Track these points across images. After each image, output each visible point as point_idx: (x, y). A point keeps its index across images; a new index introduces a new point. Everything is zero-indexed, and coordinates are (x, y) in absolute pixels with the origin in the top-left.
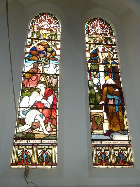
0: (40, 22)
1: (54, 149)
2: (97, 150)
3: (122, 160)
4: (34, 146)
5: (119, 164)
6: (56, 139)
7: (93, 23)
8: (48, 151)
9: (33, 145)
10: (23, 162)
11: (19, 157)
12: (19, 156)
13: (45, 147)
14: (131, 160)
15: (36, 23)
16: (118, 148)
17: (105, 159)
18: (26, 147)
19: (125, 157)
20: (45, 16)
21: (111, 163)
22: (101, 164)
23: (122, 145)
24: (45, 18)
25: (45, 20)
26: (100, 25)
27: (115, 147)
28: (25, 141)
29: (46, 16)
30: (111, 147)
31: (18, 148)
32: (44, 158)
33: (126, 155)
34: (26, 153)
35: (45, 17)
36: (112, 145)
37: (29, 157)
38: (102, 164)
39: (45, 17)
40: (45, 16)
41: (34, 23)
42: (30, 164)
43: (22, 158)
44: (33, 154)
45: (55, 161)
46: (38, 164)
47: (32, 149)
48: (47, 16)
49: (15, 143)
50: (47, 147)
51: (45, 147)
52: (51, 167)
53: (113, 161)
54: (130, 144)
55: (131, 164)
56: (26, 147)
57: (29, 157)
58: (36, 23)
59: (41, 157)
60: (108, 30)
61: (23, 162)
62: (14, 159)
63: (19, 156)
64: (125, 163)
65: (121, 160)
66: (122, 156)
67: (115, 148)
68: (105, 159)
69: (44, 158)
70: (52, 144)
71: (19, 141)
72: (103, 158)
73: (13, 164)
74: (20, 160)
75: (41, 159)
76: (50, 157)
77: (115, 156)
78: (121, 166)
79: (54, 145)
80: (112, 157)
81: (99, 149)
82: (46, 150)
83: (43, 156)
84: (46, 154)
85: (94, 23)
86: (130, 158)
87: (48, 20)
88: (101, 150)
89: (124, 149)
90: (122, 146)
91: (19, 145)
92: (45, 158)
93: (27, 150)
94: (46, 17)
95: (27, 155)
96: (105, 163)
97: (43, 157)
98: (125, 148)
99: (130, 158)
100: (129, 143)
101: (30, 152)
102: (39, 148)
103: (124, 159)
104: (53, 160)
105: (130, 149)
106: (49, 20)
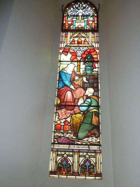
0: (73, 10)
1: (98, 156)
2: (80, 156)
3: (87, 169)
4: (74, 152)
5: (83, 174)
6: (100, 145)
7: (87, 6)
8: (91, 158)
9: (73, 151)
10: (63, 171)
11: (58, 164)
12: (58, 163)
13: (87, 154)
14: (100, 170)
15: (70, 12)
16: (63, 153)
17: (67, 167)
18: (65, 153)
19: (92, 166)
20: (79, 3)
21: (74, 172)
22: (61, 172)
23: (63, 150)
24: (79, 6)
25: (79, 8)
26: (82, 8)
27: (59, 151)
28: (66, 147)
29: (80, 4)
30: (54, 151)
31: (79, 155)
32: (87, 167)
33: (93, 163)
34: (65, 160)
35: (79, 5)
36: (77, 151)
37: (69, 165)
38: (62, 173)
39: (79, 5)
40: (79, 3)
41: (68, 13)
42: (71, 174)
43: (62, 166)
44: (74, 162)
45: (55, 169)
46: (80, 174)
47: (80, 156)
48: (82, 4)
49: (53, 148)
50: (67, 153)
51: (87, 154)
52: (86, 178)
53: (76, 170)
54: (100, 150)
55: (100, 175)
56: (65, 153)
57: (69, 165)
58: (70, 12)
59: (83, 166)
60: (90, 13)
61: (93, 171)
62: (52, 166)
63: (58, 163)
64: (90, 174)
65: (86, 170)
66: (89, 164)
67: (59, 153)
68: (67, 167)
69: (87, 167)
70: (95, 150)
71: (56, 147)
72: (63, 166)
73: (52, 173)
74: (83, 169)
75: (84, 168)
76: (94, 166)
77: (57, 162)
78: (66, 176)
79: (98, 151)
80: (76, 165)
81: (61, 154)
82: (89, 158)
83: (86, 164)
84: (89, 162)
85: (75, 6)
86: (99, 166)
87: (82, 8)
88: (63, 156)
89: (70, 155)
90: (68, 152)
91: (58, 150)
92: (88, 167)
93: (67, 157)
94: (81, 5)
95: (90, 162)
96: (65, 171)
97: (86, 166)
98: (71, 153)
99: (99, 166)
100: (100, 149)
101: (93, 160)
102: (81, 155)
103: (91, 168)
104: (75, 169)
105: (99, 156)
106: (84, 8)
